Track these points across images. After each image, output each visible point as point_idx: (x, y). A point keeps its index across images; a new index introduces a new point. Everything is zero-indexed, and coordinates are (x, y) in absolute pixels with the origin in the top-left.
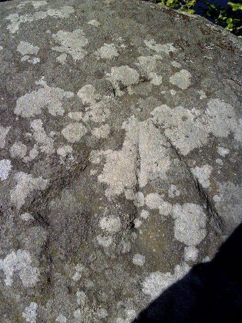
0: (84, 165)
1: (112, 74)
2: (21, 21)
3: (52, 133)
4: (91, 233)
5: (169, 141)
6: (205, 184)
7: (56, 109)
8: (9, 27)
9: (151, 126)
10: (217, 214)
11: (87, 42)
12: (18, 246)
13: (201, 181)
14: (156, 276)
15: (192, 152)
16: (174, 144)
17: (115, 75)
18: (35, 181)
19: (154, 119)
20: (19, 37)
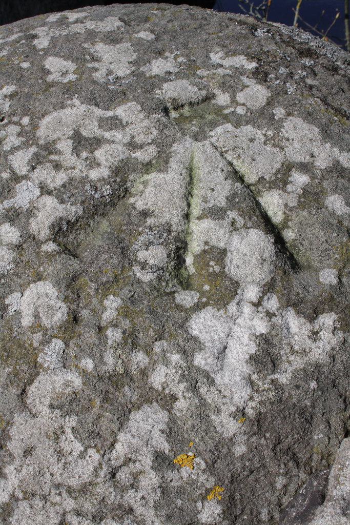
0: (121, 191)
1: (164, 91)
2: (51, 35)
3: (84, 154)
4: (127, 265)
5: (231, 164)
6: (277, 218)
7: (90, 129)
8: (36, 42)
9: (210, 150)
10: (237, 318)
11: (135, 57)
12: (39, 278)
13: (270, 213)
14: (206, 314)
15: (260, 335)
16: (238, 169)
17: (169, 91)
18: (61, 207)
19: (213, 140)
20: (47, 52)
